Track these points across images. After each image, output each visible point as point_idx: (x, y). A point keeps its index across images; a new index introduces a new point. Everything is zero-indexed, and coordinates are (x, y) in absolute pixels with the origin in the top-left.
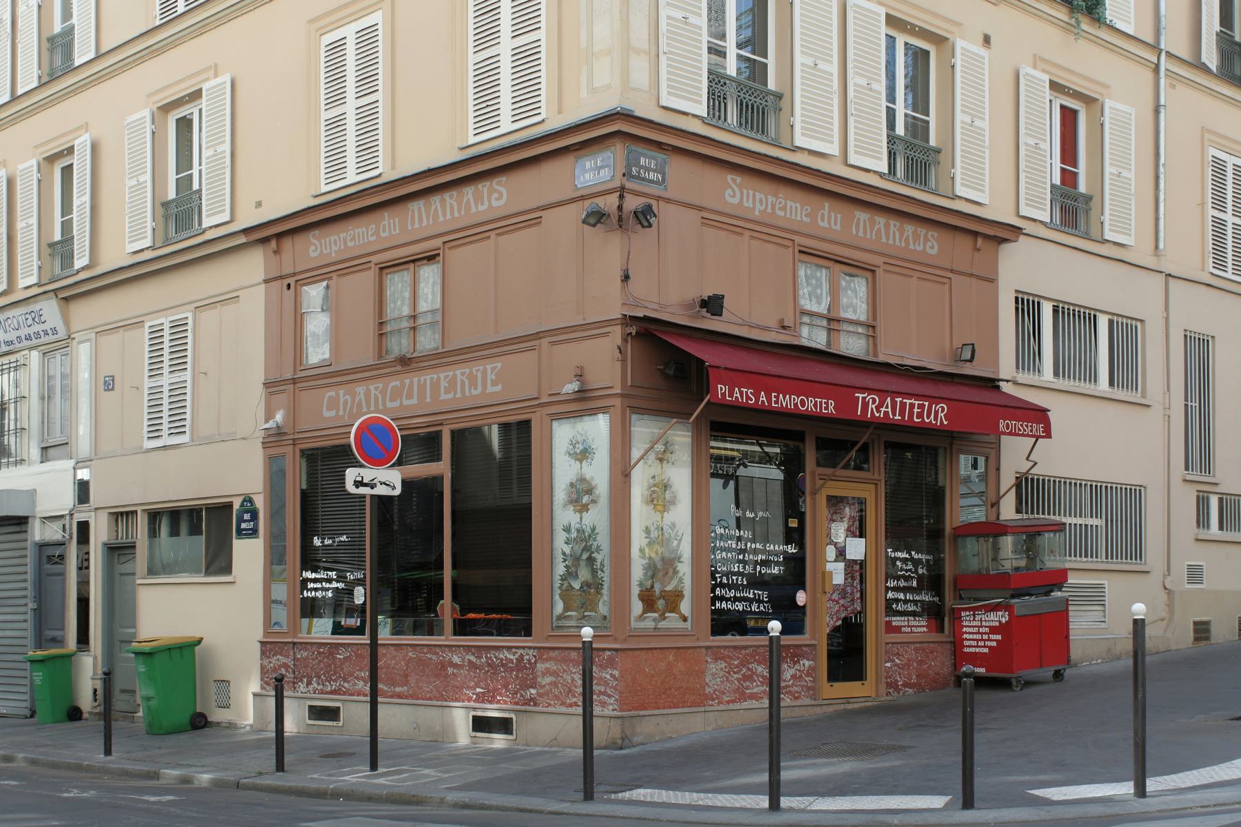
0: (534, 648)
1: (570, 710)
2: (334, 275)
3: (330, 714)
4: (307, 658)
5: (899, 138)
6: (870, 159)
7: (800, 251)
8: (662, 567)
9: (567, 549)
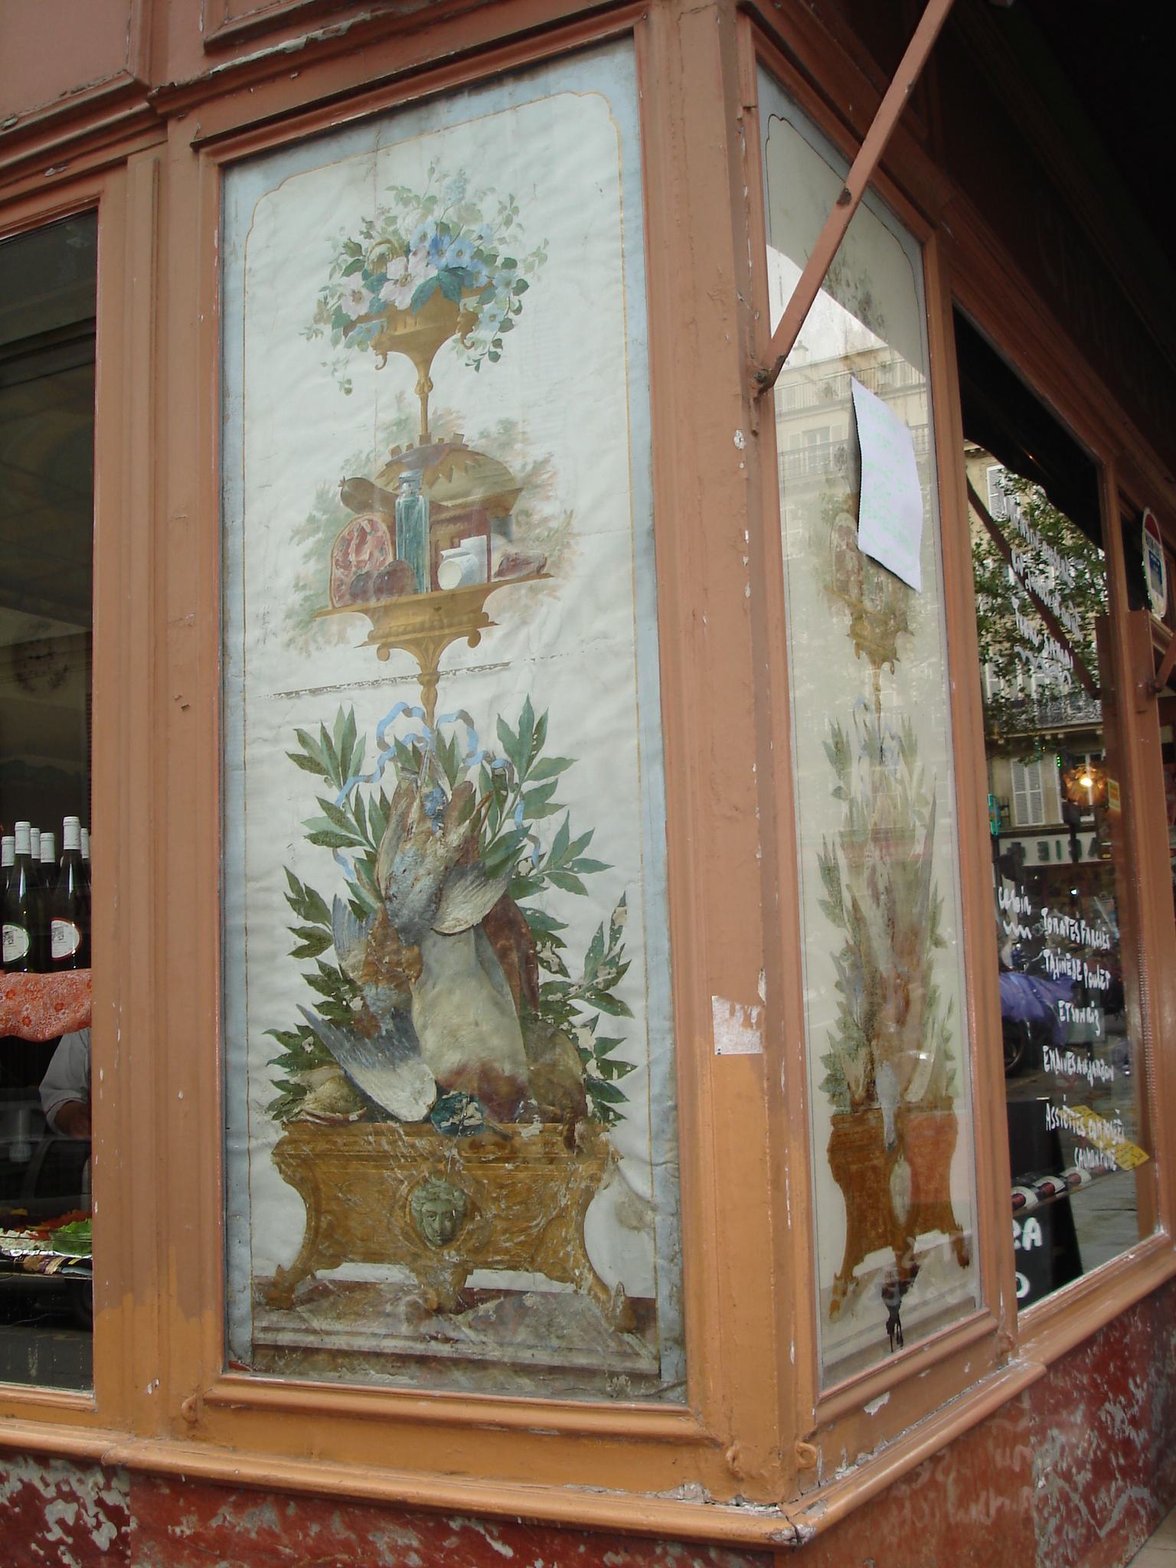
9: (333, 878)
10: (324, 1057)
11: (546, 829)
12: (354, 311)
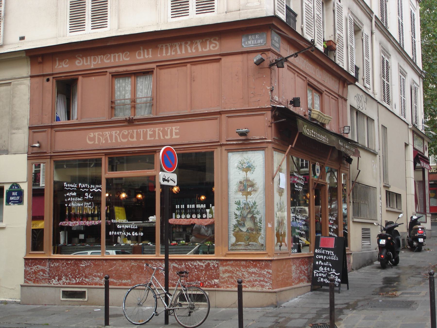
0: (217, 260)
1: (101, 286)
4: (58, 266)
9: (238, 213)
10: (237, 227)
11: (256, 210)
12: (240, 167)
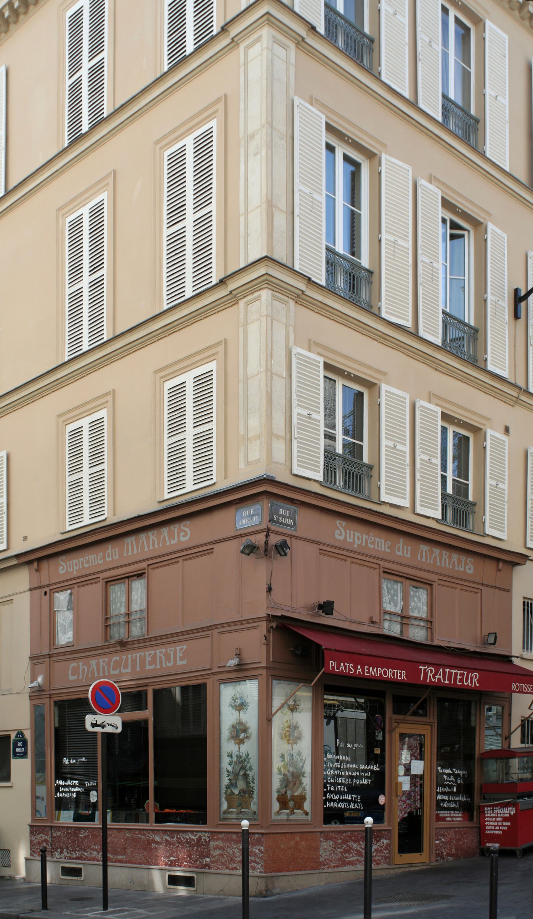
0: (209, 832)
2: (76, 586)
3: (77, 872)
4: (60, 836)
5: (449, 495)
6: (430, 510)
7: (384, 572)
8: (292, 779)
9: (230, 768)
